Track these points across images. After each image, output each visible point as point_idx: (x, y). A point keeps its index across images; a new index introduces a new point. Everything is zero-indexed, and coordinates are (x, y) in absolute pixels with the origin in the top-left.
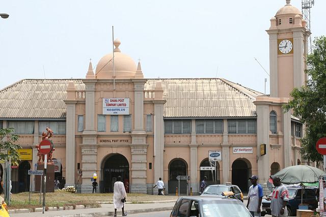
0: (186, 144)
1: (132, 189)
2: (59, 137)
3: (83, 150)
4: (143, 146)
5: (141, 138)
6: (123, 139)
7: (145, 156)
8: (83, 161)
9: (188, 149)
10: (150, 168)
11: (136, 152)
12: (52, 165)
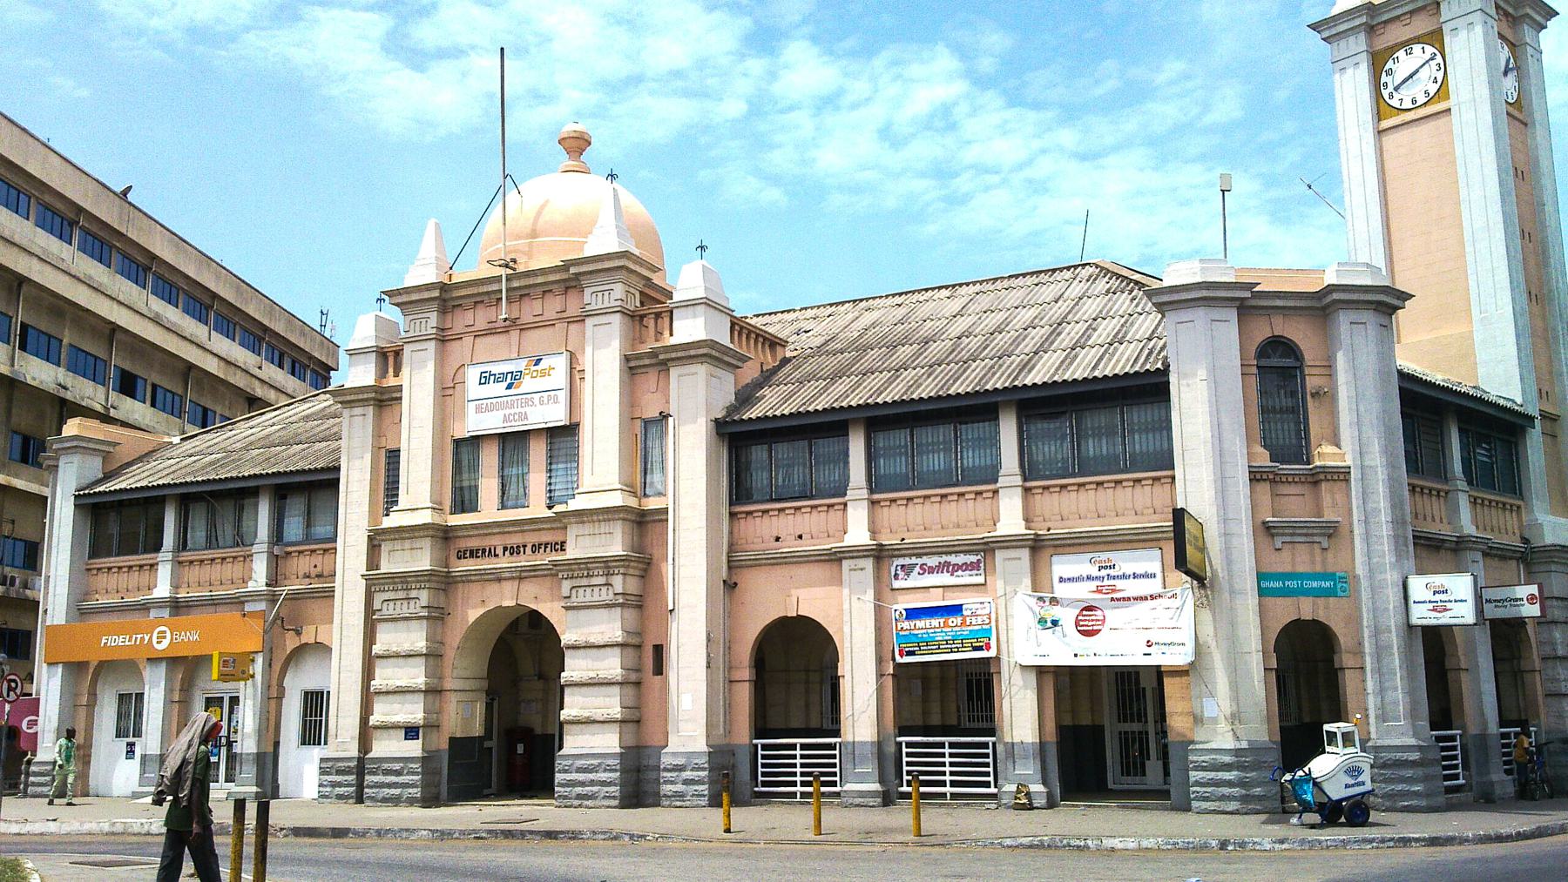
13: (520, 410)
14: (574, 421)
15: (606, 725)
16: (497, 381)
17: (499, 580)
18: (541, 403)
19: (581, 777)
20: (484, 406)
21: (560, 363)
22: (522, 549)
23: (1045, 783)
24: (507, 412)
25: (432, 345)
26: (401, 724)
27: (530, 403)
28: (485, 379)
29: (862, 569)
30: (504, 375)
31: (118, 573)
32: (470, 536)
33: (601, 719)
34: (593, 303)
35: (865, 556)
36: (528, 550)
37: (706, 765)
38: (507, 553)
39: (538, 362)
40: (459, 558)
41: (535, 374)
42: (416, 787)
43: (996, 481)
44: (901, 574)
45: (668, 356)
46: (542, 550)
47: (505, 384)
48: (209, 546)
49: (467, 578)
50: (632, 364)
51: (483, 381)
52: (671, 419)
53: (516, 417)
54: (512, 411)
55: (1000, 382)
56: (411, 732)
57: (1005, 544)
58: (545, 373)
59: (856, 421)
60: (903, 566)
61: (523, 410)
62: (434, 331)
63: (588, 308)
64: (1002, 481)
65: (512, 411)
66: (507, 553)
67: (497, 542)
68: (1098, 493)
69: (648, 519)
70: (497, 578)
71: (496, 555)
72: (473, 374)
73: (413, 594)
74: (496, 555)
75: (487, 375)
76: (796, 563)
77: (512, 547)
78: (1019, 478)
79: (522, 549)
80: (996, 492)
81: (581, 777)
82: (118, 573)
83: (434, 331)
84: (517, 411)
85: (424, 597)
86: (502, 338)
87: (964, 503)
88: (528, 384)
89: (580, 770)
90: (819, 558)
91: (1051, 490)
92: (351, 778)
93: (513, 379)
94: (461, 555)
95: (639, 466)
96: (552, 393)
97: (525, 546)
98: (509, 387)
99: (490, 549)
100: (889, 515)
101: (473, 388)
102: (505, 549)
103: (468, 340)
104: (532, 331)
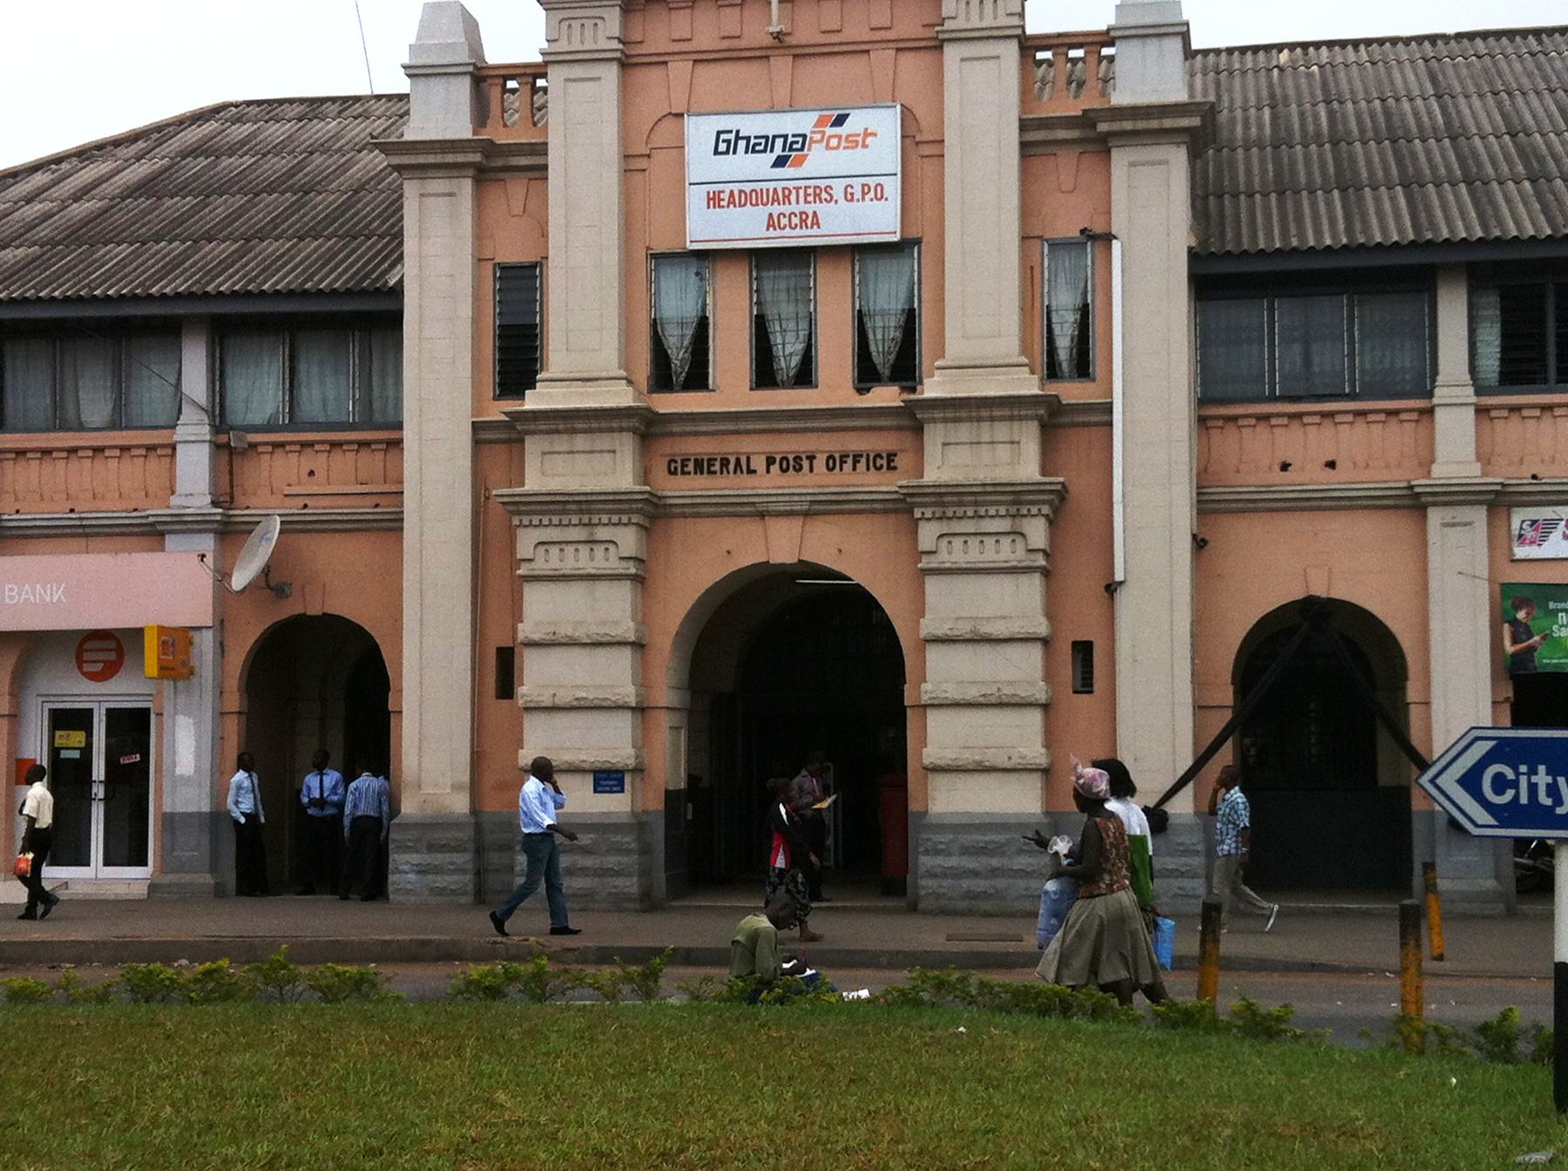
0: (1394, 478)
1: (926, 862)
2: (363, 444)
3: (526, 542)
4: (1016, 498)
5: (1002, 431)
6: (855, 443)
7: (1037, 579)
8: (526, 630)
9: (1397, 526)
10: (1085, 683)
11: (956, 554)
12: (362, 974)
13: (802, 207)
14: (913, 234)
15: (1014, 777)
16: (751, 149)
17: (762, 515)
18: (850, 198)
19: (969, 863)
20: (725, 196)
21: (884, 124)
22: (806, 464)
23: (213, 870)
24: (776, 209)
25: (611, 73)
26: (586, 766)
27: (824, 195)
28: (726, 144)
29: (1466, 524)
30: (768, 142)
31: (93, 458)
32: (696, 434)
33: (1007, 765)
34: (962, 15)
35: (1470, 503)
36: (820, 463)
37: (633, 846)
38: (775, 468)
39: (840, 121)
40: (672, 473)
41: (834, 142)
42: (630, 875)
43: (1430, 395)
44: (1530, 533)
45: (1116, 126)
46: (848, 466)
47: (772, 157)
48: (114, 425)
49: (696, 511)
50: (1033, 136)
51: (722, 147)
52: (1116, 245)
53: (795, 220)
54: (786, 209)
55: (157, 287)
56: (607, 779)
57: (310, 527)
58: (855, 142)
59: (1451, 269)
60: (1534, 522)
61: (810, 209)
62: (615, 45)
63: (949, 25)
64: (1440, 395)
65: (786, 209)
66: (775, 468)
67: (755, 447)
68: (275, 456)
69: (1066, 419)
70: (760, 513)
71: (751, 472)
72: (700, 132)
73: (602, 533)
74: (751, 472)
75: (732, 137)
76: (1331, 509)
77: (786, 458)
78: (1471, 390)
79: (806, 464)
80: (1429, 412)
81: (969, 863)
82: (93, 458)
83: (615, 45)
84: (794, 208)
85: (628, 540)
86: (753, 70)
87: (1365, 425)
88: (818, 161)
89: (965, 851)
90: (124, 530)
91: (1526, 413)
92: (464, 859)
93: (790, 151)
94: (677, 467)
95: (1037, 323)
96: (872, 182)
97: (811, 458)
98: (780, 162)
99: (738, 461)
100: (1509, 432)
101: (702, 163)
102: (770, 461)
103: (679, 69)
104: (819, 60)
